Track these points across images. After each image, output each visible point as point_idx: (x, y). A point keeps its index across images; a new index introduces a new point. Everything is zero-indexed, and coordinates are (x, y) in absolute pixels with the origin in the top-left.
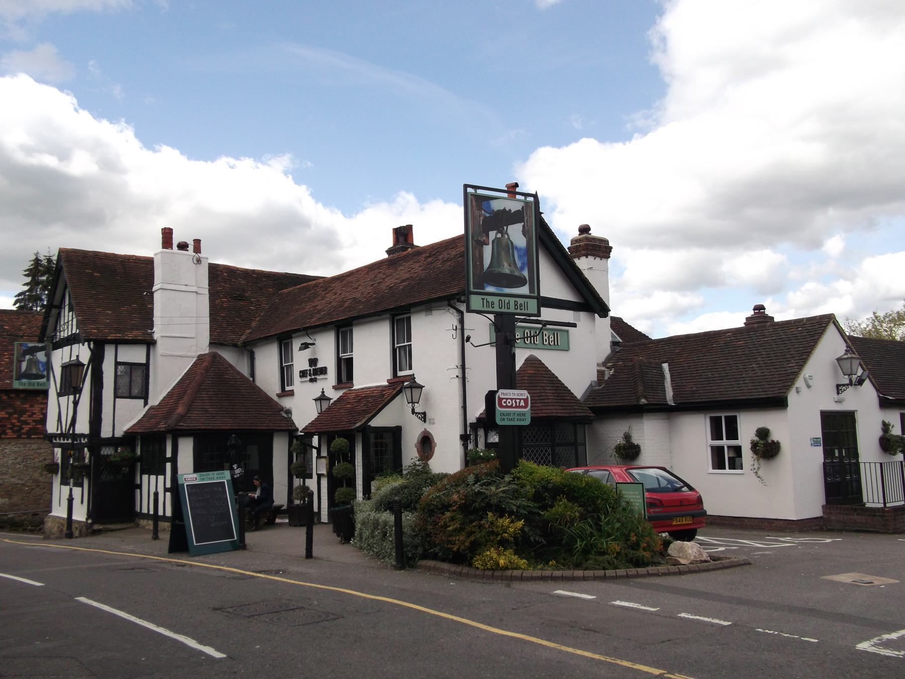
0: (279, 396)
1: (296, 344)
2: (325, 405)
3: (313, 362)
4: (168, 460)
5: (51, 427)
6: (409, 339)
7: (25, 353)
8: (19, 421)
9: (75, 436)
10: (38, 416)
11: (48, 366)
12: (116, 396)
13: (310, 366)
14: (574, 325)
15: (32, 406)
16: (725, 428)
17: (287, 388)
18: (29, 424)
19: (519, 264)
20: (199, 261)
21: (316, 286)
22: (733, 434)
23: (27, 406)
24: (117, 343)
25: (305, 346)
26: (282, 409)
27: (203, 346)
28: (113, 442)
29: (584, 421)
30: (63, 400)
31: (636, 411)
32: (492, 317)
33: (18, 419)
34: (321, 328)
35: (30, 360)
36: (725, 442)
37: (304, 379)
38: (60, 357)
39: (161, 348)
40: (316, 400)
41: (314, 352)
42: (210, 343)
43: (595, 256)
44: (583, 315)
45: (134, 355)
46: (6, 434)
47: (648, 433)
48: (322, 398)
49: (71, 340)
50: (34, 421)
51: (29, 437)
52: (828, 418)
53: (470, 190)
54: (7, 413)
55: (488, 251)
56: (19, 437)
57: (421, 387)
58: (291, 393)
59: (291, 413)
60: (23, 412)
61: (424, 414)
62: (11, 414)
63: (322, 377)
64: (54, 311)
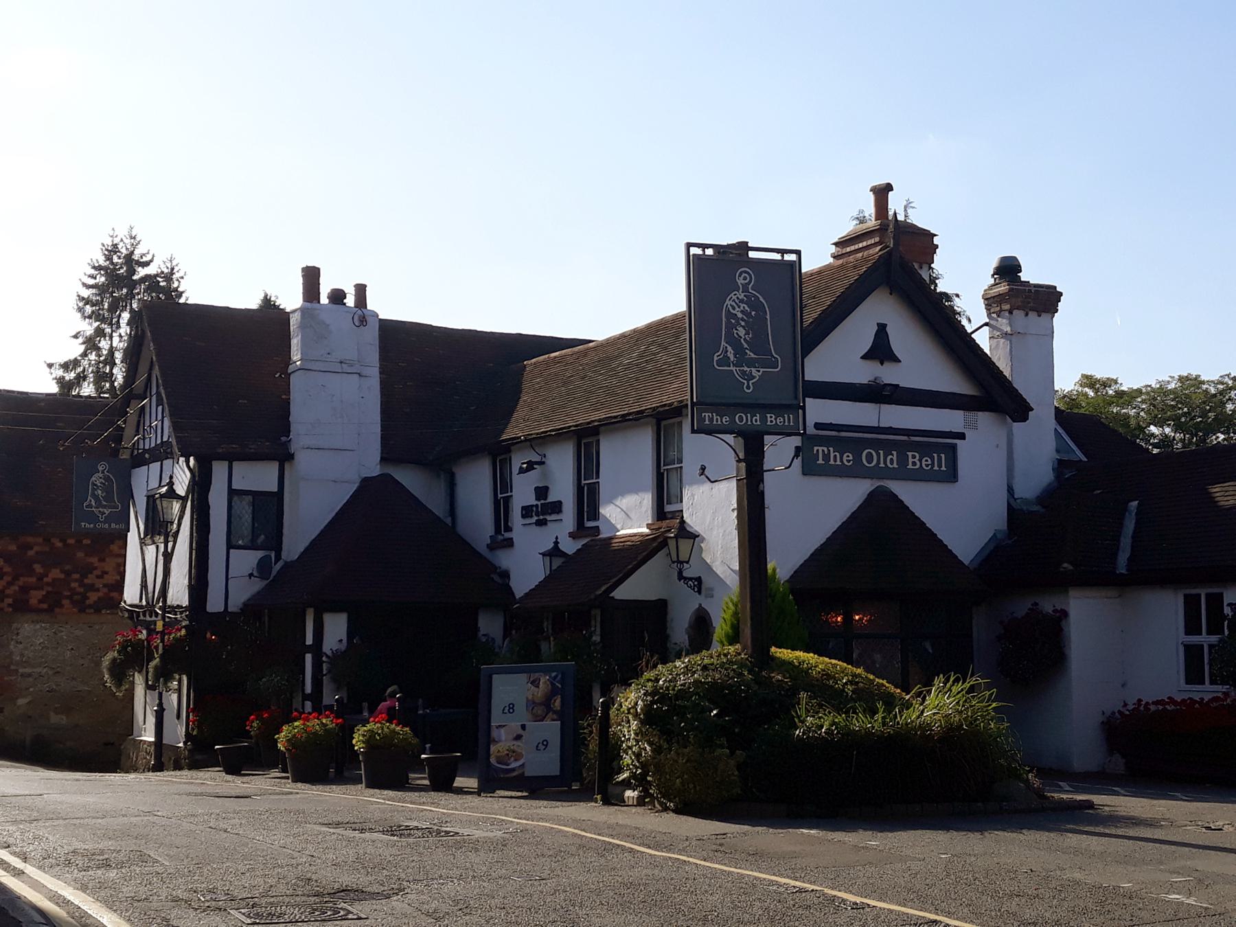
2: (557, 562)
3: (542, 492)
4: (308, 649)
5: (131, 594)
6: (598, 477)
8: (82, 585)
10: (111, 578)
12: (230, 546)
13: (538, 499)
14: (962, 436)
15: (102, 560)
17: (668, 508)
18: (98, 590)
21: (585, 353)
23: (94, 560)
24: (231, 458)
26: (494, 568)
30: (151, 551)
33: (81, 582)
37: (528, 521)
38: (145, 480)
39: (305, 461)
40: (544, 554)
41: (545, 475)
42: (383, 459)
45: (258, 476)
46: (62, 606)
47: (1086, 617)
48: (555, 552)
49: (161, 454)
50: (105, 586)
51: (98, 611)
53: (694, 251)
54: (62, 572)
56: (82, 610)
57: (694, 536)
58: (509, 543)
59: (508, 577)
61: (699, 579)
63: (554, 517)
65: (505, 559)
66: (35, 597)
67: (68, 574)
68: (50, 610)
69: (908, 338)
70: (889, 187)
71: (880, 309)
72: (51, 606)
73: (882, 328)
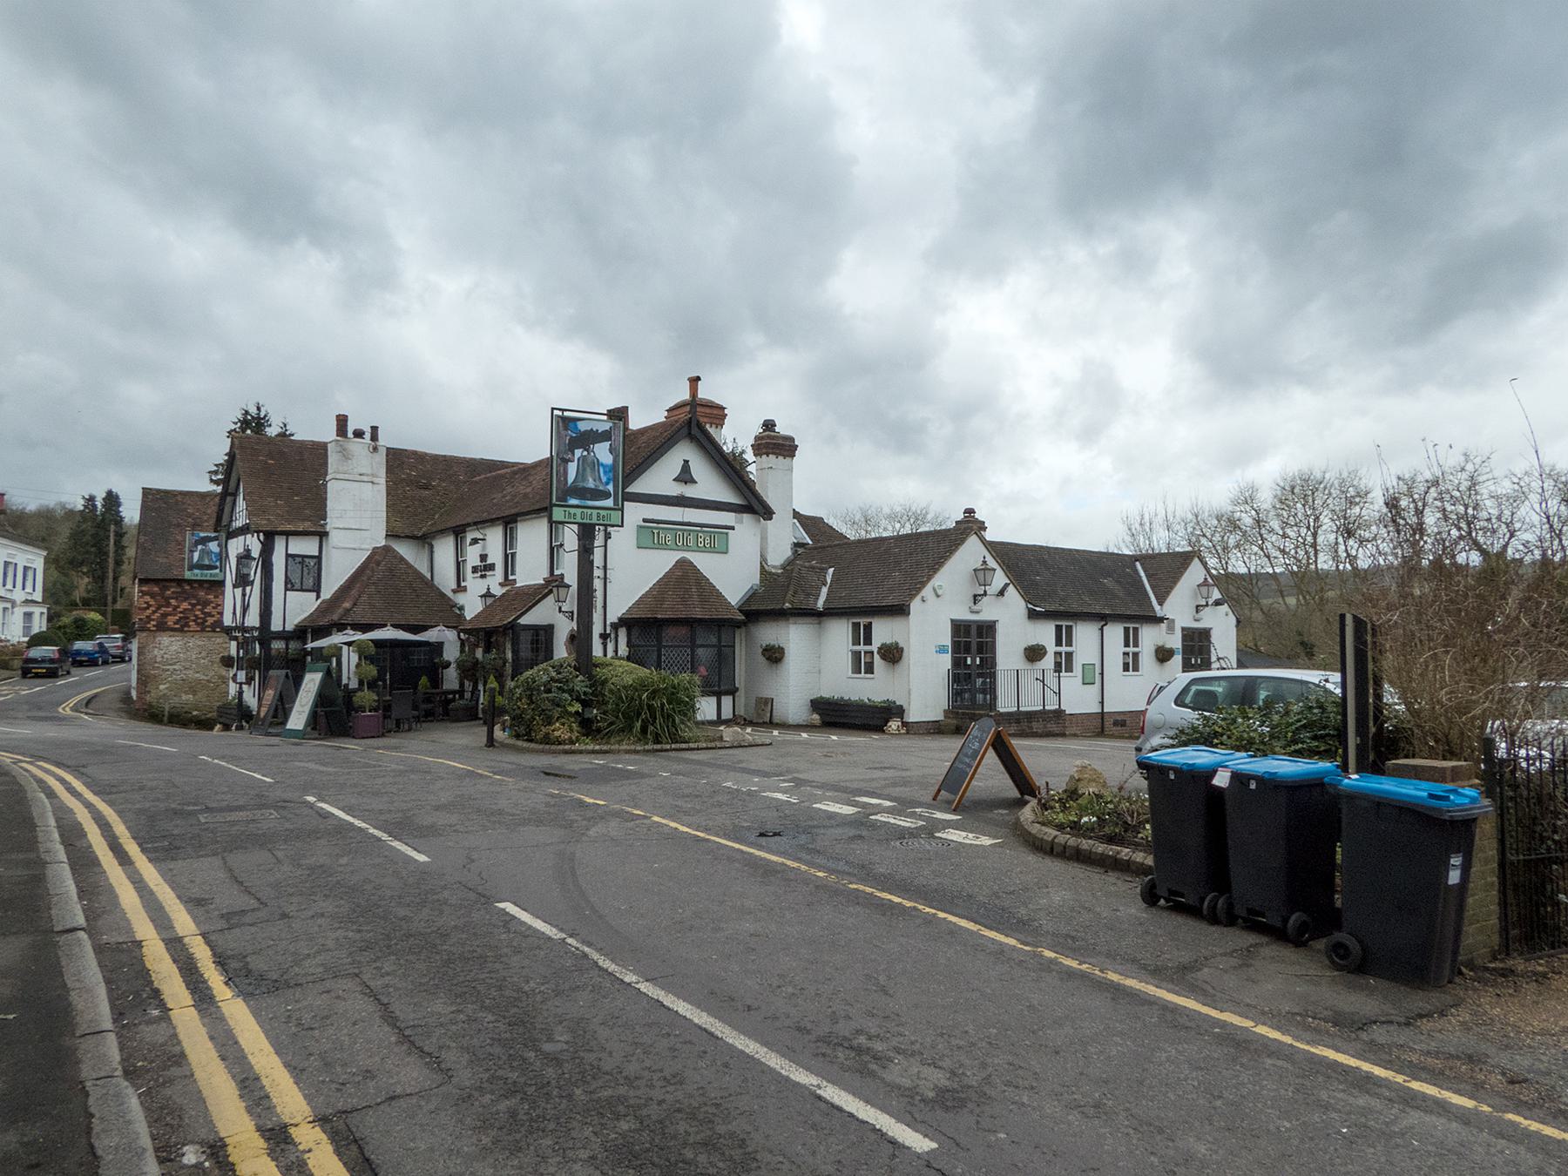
0: (454, 591)
1: (469, 536)
2: (490, 601)
3: (483, 557)
7: (197, 543)
9: (244, 629)
11: (223, 556)
16: (864, 635)
19: (604, 479)
20: (375, 449)
22: (868, 641)
23: (211, 597)
24: (288, 534)
25: (475, 541)
27: (376, 537)
28: (284, 636)
29: (735, 625)
31: (780, 615)
32: (575, 527)
34: (492, 522)
35: (583, 459)
36: (862, 648)
38: (235, 547)
39: (335, 538)
41: (484, 547)
43: (777, 455)
44: (746, 517)
47: (794, 637)
48: (488, 595)
49: (244, 530)
52: (959, 628)
55: (572, 469)
56: (203, 630)
58: (465, 589)
60: (206, 603)
62: (193, 605)
64: (229, 499)
65: (461, 599)
66: (171, 621)
67: (193, 605)
68: (181, 630)
69: (701, 469)
70: (698, 379)
71: (683, 453)
72: (182, 628)
73: (686, 462)
